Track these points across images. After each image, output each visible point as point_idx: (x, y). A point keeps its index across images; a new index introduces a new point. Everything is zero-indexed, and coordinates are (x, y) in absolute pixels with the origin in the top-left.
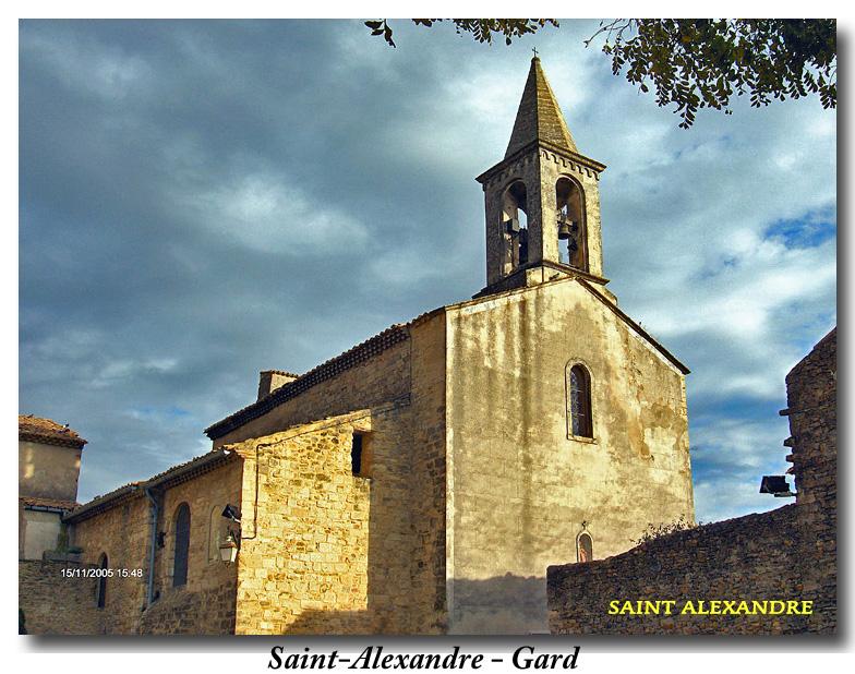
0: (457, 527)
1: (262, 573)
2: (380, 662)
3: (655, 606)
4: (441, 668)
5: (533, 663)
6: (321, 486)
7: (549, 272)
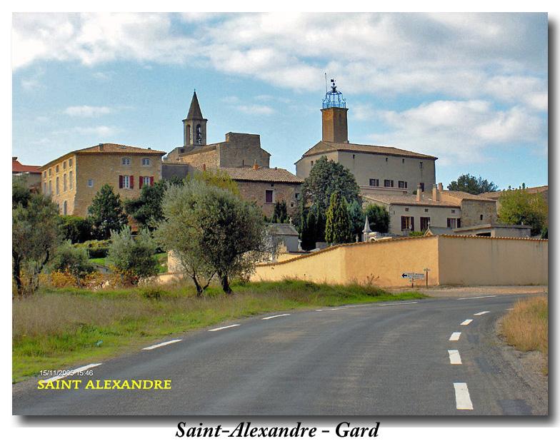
2: (249, 433)
3: (68, 383)
4: (289, 436)
5: (349, 433)
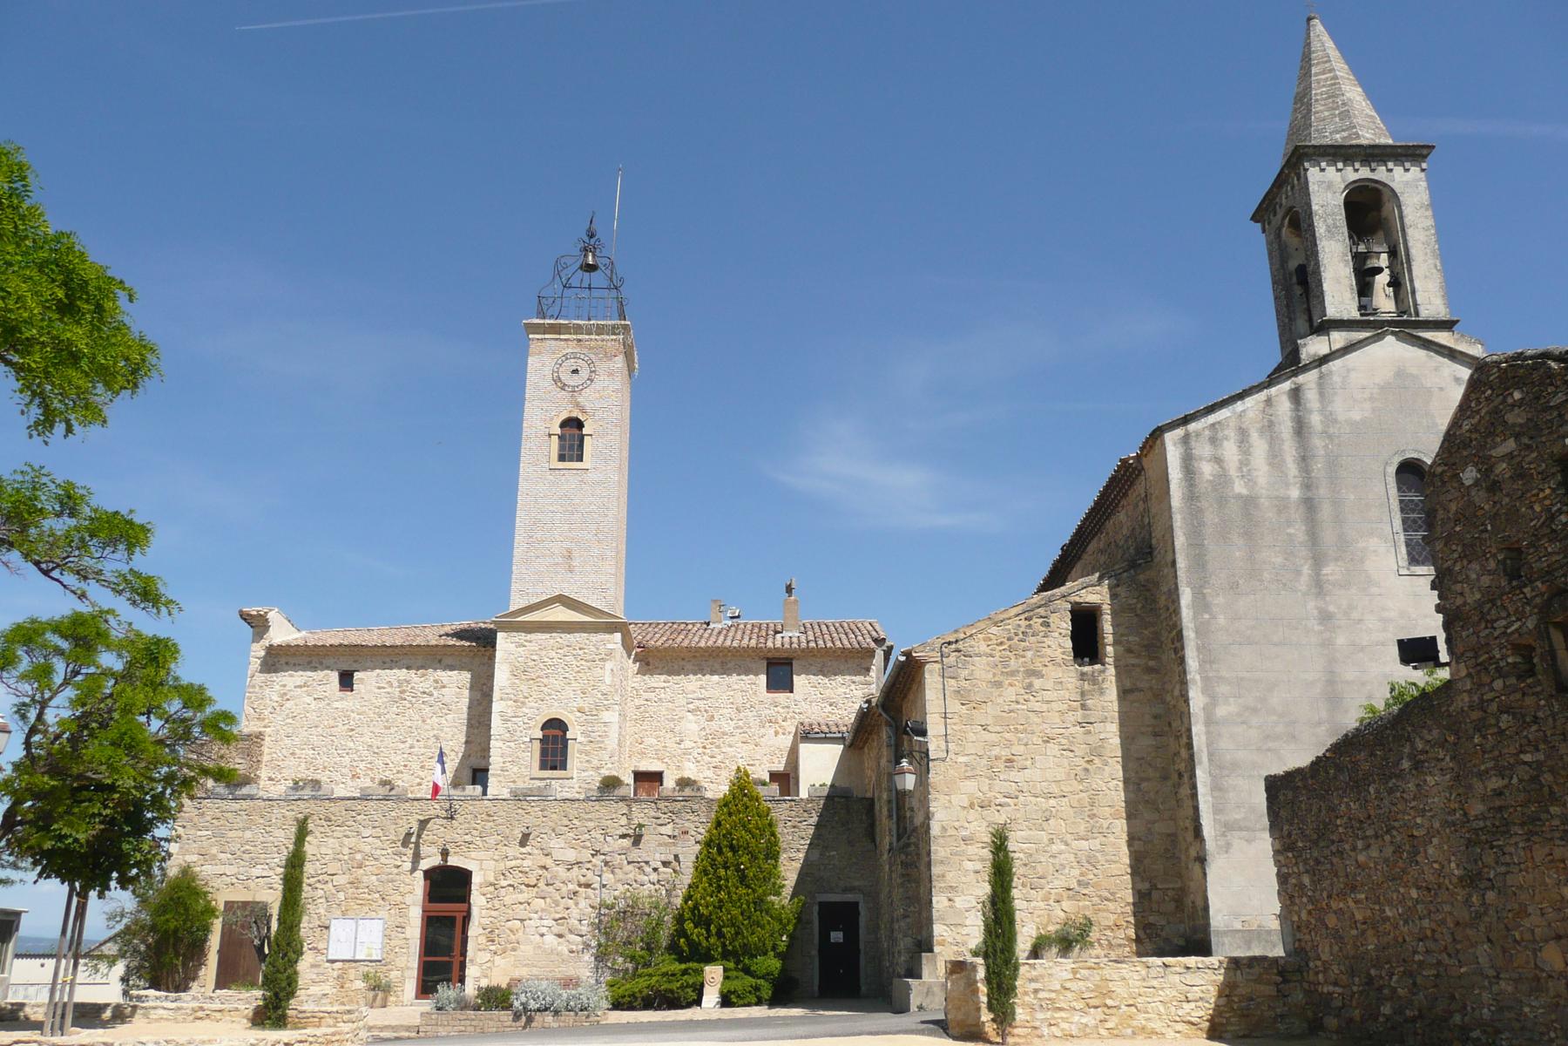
0: (1209, 721)
1: (960, 799)
6: (1030, 685)
7: (1339, 338)
